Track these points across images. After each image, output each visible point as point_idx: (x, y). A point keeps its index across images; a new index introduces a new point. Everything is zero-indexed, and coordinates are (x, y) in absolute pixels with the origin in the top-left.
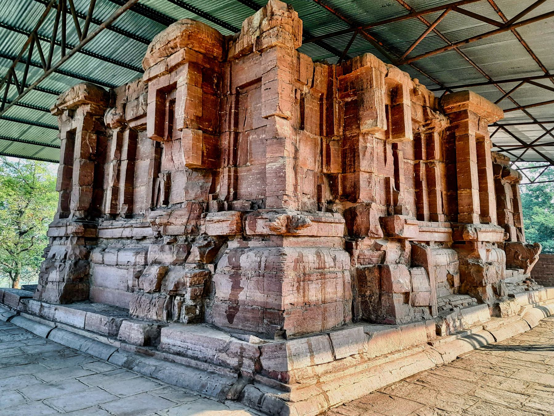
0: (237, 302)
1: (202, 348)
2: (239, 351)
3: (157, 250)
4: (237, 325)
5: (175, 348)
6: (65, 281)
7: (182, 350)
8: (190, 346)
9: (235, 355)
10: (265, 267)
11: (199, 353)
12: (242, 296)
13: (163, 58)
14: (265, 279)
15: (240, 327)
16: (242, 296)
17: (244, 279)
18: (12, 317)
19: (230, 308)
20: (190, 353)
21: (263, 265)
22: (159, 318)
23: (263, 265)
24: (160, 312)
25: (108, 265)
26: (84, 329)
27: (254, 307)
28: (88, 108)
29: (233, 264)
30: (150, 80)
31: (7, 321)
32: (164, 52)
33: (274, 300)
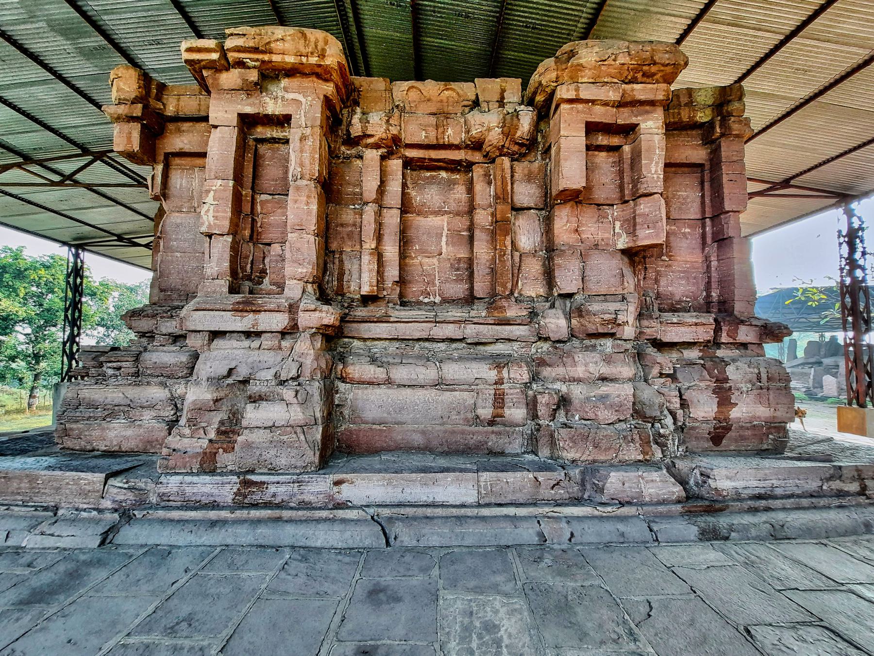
0: (727, 419)
1: (798, 482)
2: (856, 474)
3: (599, 360)
4: (729, 446)
5: (750, 492)
6: (320, 421)
7: (762, 491)
8: (776, 482)
9: (853, 479)
10: (768, 378)
11: (795, 488)
12: (735, 413)
13: (616, 80)
14: (771, 392)
15: (732, 448)
16: (735, 413)
17: (737, 393)
18: (113, 529)
19: (715, 429)
20: (779, 492)
21: (764, 376)
22: (648, 457)
23: (764, 376)
24: (647, 449)
25: (399, 386)
26: (479, 506)
27: (755, 423)
28: (719, 118)
29: (717, 377)
30: (416, 88)
31: (102, 543)
32: (626, 73)
33: (784, 414)
